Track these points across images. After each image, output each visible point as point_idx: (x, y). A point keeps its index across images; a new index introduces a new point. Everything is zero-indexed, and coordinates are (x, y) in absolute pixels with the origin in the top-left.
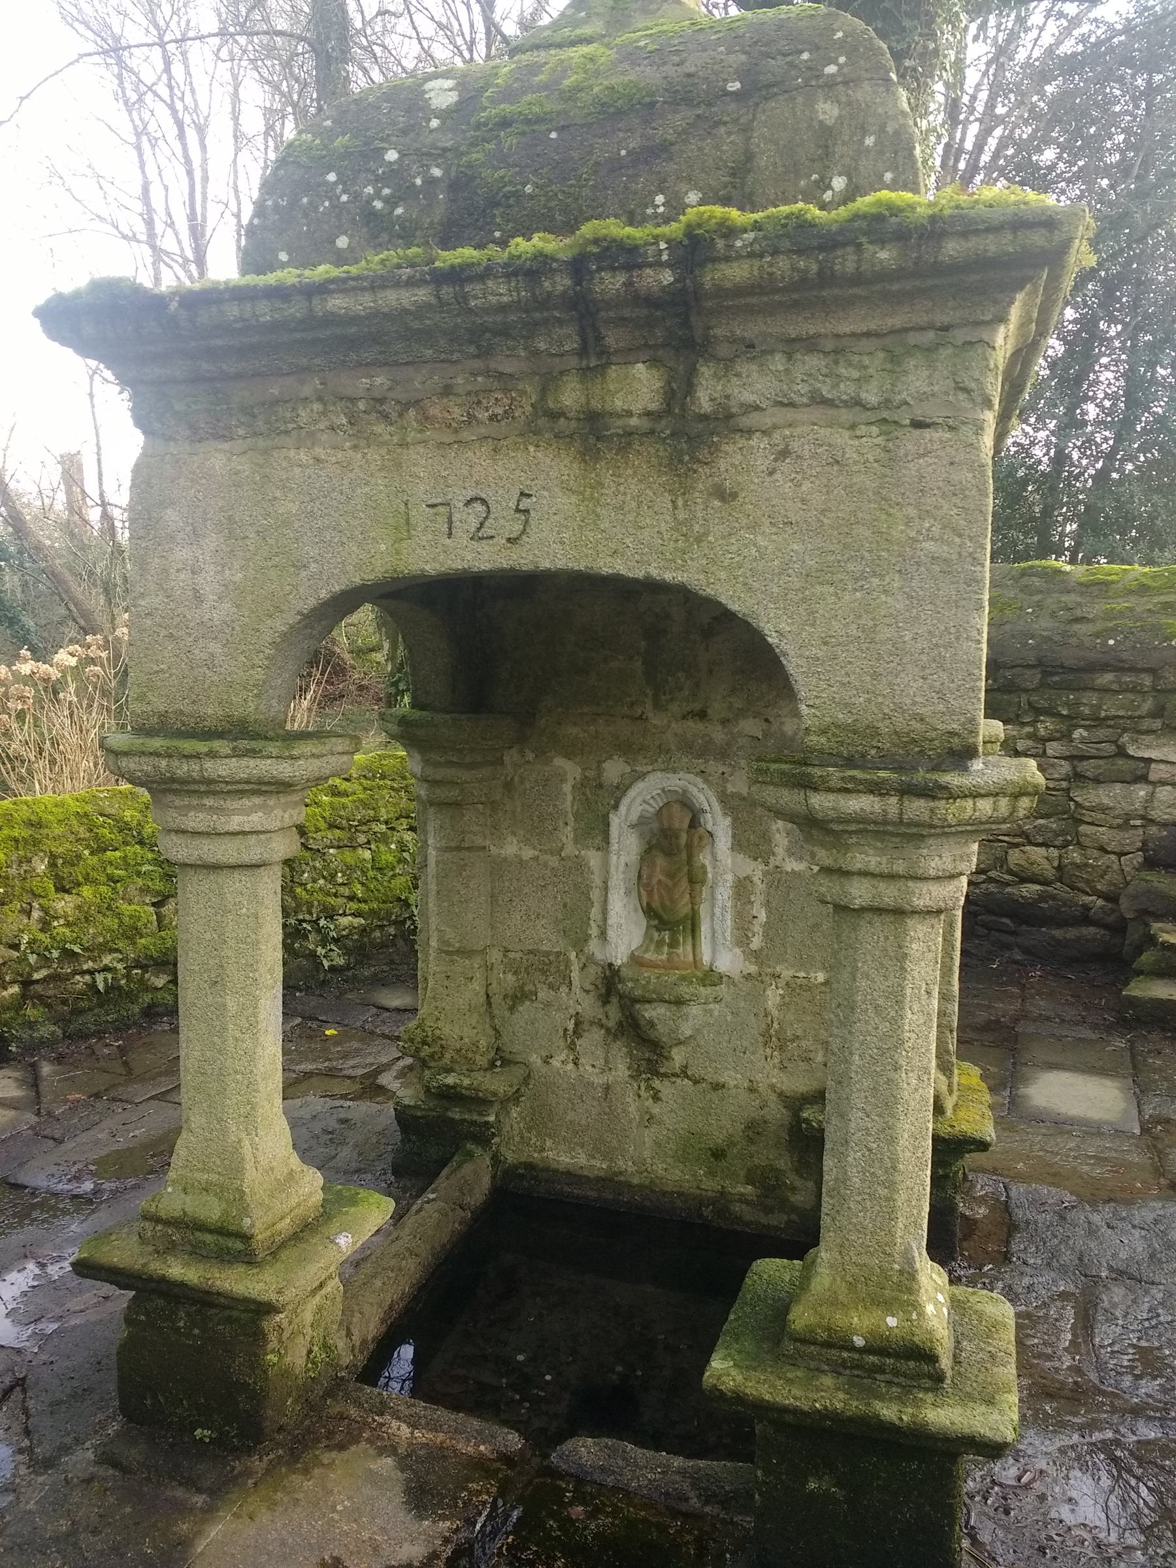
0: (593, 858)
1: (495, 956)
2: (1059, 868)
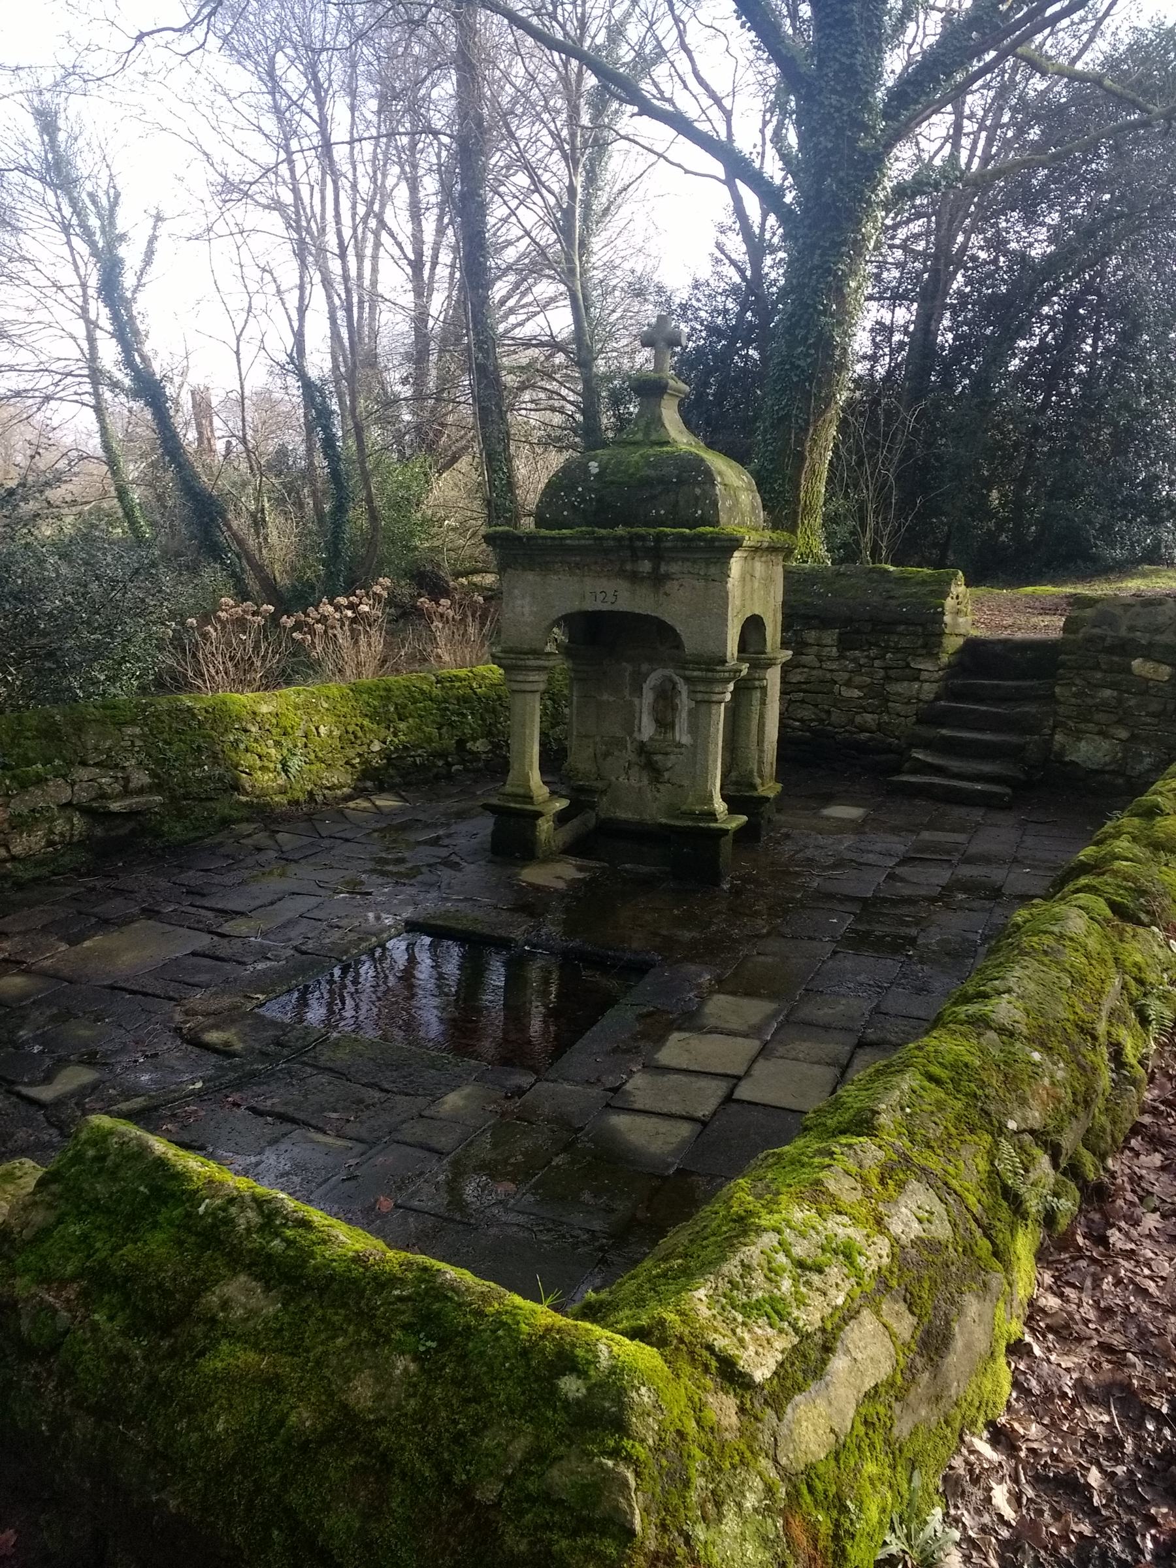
0: (636, 701)
1: (598, 739)
2: (879, 724)
